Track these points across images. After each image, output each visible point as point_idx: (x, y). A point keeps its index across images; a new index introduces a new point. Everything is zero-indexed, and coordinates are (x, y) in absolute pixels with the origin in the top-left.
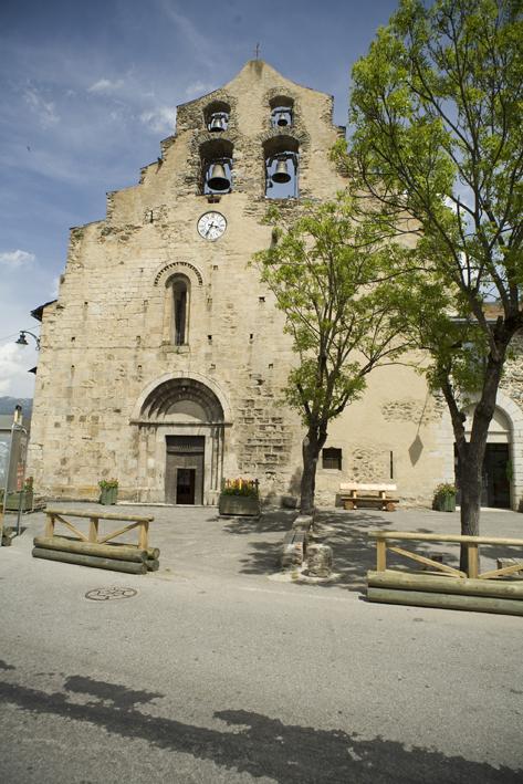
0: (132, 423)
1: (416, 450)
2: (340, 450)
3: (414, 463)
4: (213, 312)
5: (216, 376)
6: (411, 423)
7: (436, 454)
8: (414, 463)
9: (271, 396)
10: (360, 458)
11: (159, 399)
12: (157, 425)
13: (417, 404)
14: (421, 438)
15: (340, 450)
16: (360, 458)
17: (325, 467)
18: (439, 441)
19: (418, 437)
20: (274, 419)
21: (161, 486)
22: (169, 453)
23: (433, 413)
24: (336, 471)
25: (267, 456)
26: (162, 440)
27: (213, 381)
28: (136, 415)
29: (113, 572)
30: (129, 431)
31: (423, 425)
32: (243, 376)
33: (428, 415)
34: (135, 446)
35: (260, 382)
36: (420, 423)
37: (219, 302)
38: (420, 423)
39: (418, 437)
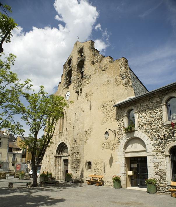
0: (55, 157)
1: (111, 160)
2: (91, 162)
3: (111, 166)
4: (67, 121)
5: (67, 141)
6: (110, 150)
7: (117, 163)
8: (111, 166)
9: (77, 145)
10: (96, 165)
11: (60, 149)
12: (61, 157)
13: (111, 142)
14: (113, 156)
15: (91, 162)
16: (96, 165)
17: (31, 182)
18: (118, 157)
19: (112, 155)
20: (77, 152)
21: (62, 175)
22: (65, 165)
23: (117, 145)
24: (2, 143)
25: (76, 165)
26: (62, 161)
27: (67, 142)
28: (55, 154)
29: (174, 83)
30: (54, 158)
31: (113, 151)
32: (72, 140)
33: (115, 146)
34: (55, 163)
35: (75, 141)
36: (112, 150)
37: (68, 118)
38: (112, 150)
39: (112, 155)
